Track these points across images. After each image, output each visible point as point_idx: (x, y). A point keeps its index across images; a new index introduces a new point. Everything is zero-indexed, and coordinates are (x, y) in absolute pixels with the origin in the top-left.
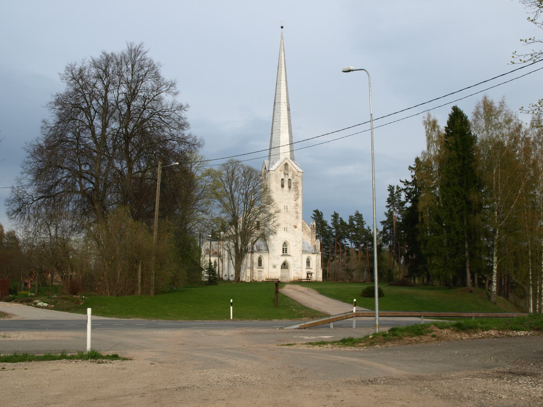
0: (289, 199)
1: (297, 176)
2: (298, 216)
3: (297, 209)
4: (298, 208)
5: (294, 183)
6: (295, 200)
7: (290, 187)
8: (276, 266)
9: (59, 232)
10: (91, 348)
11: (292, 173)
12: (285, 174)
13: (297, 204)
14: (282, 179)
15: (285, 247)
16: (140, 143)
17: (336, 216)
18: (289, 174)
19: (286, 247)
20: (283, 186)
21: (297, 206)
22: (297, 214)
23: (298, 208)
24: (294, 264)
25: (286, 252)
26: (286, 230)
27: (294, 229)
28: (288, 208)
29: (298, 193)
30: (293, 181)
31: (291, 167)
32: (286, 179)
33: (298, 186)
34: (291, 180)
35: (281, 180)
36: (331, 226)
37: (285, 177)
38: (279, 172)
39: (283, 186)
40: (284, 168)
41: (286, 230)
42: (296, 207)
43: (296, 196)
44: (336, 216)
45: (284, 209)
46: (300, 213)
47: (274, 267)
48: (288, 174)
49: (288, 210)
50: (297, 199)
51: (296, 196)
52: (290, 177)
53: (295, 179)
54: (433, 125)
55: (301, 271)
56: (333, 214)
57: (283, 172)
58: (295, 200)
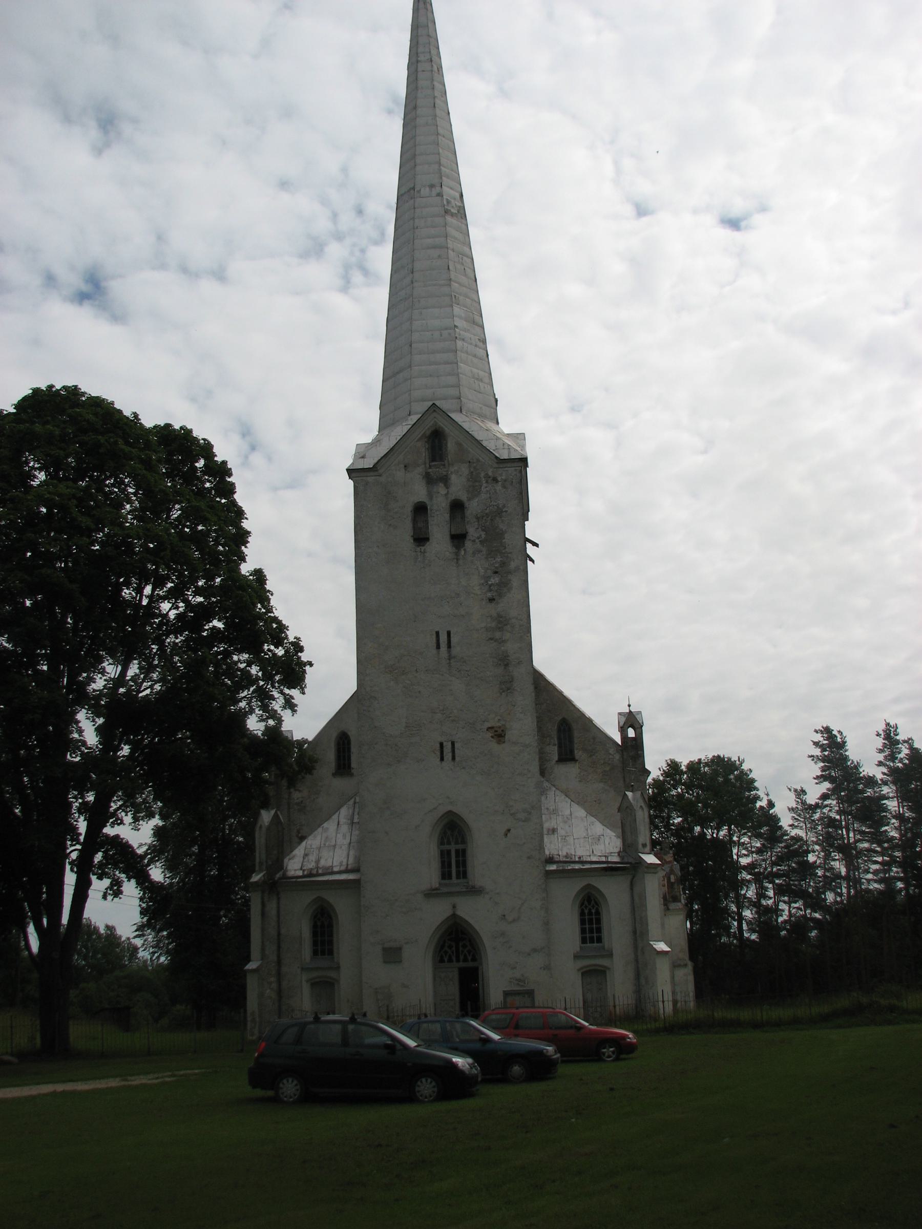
0: (458, 595)
1: (495, 480)
2: (511, 680)
3: (504, 641)
4: (507, 636)
5: (478, 518)
6: (491, 600)
7: (458, 539)
8: (400, 949)
9: (193, 600)
10: (464, 511)
11: (465, 470)
12: (429, 480)
13: (499, 616)
14: (420, 510)
15: (453, 848)
16: (394, 518)
17: (890, 737)
18: (453, 478)
19: (460, 847)
20: (421, 539)
21: (500, 629)
22: (507, 665)
23: (507, 636)
24: (503, 934)
25: (463, 874)
26: (448, 755)
27: (494, 746)
28: (454, 640)
29: (503, 564)
30: (473, 507)
31: (459, 445)
32: (439, 505)
33: (502, 527)
34: (466, 505)
35: (409, 509)
36: (878, 773)
37: (430, 495)
38: (400, 475)
39: (421, 539)
40: (424, 454)
41: (448, 755)
42: (498, 635)
43: (495, 580)
44: (890, 737)
45: (434, 651)
46: (520, 663)
47: (392, 954)
48: (445, 480)
49: (456, 650)
50: (500, 595)
51: (495, 580)
52: (458, 486)
53: (483, 496)
54: (411, 543)
55: (547, 968)
56: (881, 727)
57: (420, 469)
58: (491, 600)
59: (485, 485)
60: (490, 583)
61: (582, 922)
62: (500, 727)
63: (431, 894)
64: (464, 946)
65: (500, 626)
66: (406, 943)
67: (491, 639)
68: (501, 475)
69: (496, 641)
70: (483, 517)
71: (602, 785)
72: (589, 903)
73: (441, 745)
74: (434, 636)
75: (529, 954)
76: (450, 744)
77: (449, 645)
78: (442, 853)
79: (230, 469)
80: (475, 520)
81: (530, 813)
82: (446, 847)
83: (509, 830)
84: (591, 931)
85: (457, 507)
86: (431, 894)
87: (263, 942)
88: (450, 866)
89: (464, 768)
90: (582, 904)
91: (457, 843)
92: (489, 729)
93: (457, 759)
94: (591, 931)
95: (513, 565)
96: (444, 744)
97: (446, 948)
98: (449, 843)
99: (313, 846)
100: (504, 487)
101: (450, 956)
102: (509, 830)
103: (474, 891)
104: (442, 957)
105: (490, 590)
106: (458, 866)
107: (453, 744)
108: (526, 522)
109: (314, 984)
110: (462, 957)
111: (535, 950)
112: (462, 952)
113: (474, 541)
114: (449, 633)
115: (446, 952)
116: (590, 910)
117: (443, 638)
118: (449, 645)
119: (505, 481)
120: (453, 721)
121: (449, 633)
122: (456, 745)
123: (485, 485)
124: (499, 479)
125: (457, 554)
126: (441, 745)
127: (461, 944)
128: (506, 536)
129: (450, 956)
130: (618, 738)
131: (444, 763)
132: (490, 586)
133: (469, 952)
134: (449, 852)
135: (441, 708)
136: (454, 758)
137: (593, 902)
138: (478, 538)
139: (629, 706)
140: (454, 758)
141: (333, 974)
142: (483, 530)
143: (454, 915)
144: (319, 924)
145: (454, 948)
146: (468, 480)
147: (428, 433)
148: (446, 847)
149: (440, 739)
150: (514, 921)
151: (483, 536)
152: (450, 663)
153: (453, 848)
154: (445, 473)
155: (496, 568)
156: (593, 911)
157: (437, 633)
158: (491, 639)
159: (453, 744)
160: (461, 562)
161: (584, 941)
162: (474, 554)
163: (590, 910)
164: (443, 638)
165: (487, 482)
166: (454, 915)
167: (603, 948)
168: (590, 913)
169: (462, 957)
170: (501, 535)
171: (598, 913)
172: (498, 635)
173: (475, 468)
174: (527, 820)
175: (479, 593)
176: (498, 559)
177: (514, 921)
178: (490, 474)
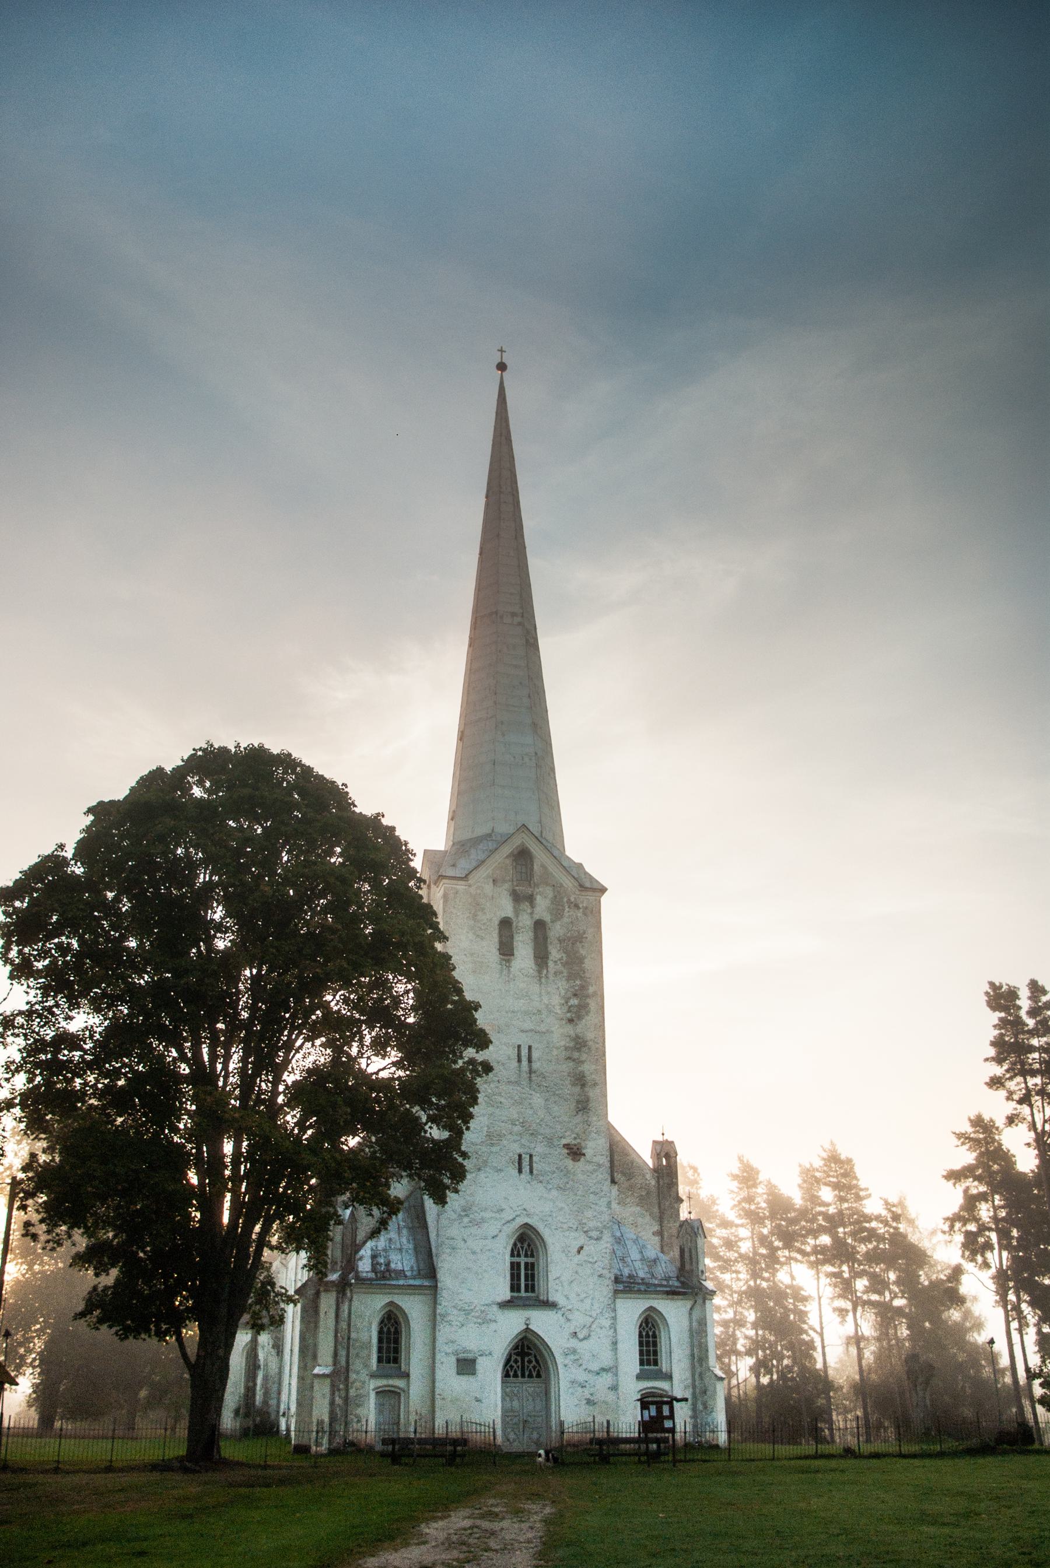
1: (577, 906)
2: (588, 1100)
3: (582, 1062)
4: (584, 1057)
6: (571, 1021)
7: (541, 957)
11: (549, 892)
12: (517, 898)
15: (523, 1260)
19: (530, 1260)
21: (579, 1050)
22: (583, 1086)
23: (584, 1057)
25: (531, 1288)
27: (569, 1163)
28: (535, 1055)
30: (556, 930)
31: (543, 866)
32: (525, 921)
33: (583, 952)
42: (576, 1055)
43: (574, 1001)
45: (517, 1064)
46: (595, 1084)
47: (466, 1366)
48: (531, 899)
49: (536, 1066)
51: (574, 1001)
52: (542, 907)
53: (566, 920)
59: (567, 909)
60: (569, 1004)
61: (641, 1344)
62: (575, 1145)
63: (505, 1305)
64: (530, 1362)
65: (578, 1046)
66: (481, 1355)
67: (569, 1058)
68: (583, 902)
69: (574, 1060)
70: (564, 940)
71: (638, 1208)
72: (647, 1326)
73: (520, 1156)
74: (516, 1050)
75: (598, 1374)
76: (528, 1156)
77: (530, 1060)
78: (512, 1264)
79: (992, 1120)
80: (557, 942)
81: (602, 1232)
82: (516, 1259)
83: (582, 1248)
84: (648, 1354)
85: (540, 926)
86: (505, 1305)
87: (336, 1347)
88: (519, 1279)
89: (541, 1182)
90: (641, 1326)
91: (526, 1256)
92: (564, 1146)
93: (535, 1172)
94: (648, 1354)
95: (591, 990)
96: (523, 1156)
97: (512, 1363)
98: (519, 1255)
99: (379, 1248)
100: (585, 914)
101: (515, 1372)
102: (582, 1248)
103: (548, 1305)
104: (507, 1371)
105: (569, 1011)
106: (526, 1280)
107: (531, 1156)
108: (168, 768)
109: (380, 1393)
110: (527, 1373)
111: (603, 1370)
112: (528, 1367)
113: (555, 962)
114: (530, 1048)
115: (512, 1367)
116: (647, 1332)
117: (524, 1052)
118: (530, 1060)
119: (586, 908)
120: (532, 1134)
121: (530, 1048)
122: (534, 1158)
123: (567, 909)
124: (581, 906)
125: (540, 972)
126: (520, 1156)
127: (526, 1359)
128: (586, 961)
129: (515, 1372)
130: (650, 1163)
131: (523, 1176)
132: (570, 1007)
133: (534, 1367)
134: (519, 1264)
135: (521, 1121)
136: (531, 1172)
137: (650, 1325)
138: (560, 960)
139: (663, 1134)
140: (531, 1172)
141: (400, 1383)
142: (565, 953)
143: (527, 1330)
144: (385, 1330)
145: (519, 1364)
146: (552, 903)
147: (516, 852)
148: (516, 1259)
149: (518, 1151)
150: (585, 1338)
151: (565, 959)
152: (530, 1077)
153: (523, 1260)
154: (530, 892)
155: (576, 990)
156: (651, 1333)
157: (519, 1047)
158: (569, 1058)
159: (531, 1156)
160: (543, 980)
161: (642, 1363)
162: (555, 973)
163: (647, 1332)
164: (524, 1052)
165: (569, 907)
166: (527, 1330)
167: (661, 1370)
168: (647, 1336)
169: (527, 1373)
170: (581, 960)
171: (654, 1336)
172: (576, 1055)
173: (558, 892)
174: (598, 1239)
175: (559, 1011)
176: (578, 982)
177: (585, 1338)
178: (573, 900)
